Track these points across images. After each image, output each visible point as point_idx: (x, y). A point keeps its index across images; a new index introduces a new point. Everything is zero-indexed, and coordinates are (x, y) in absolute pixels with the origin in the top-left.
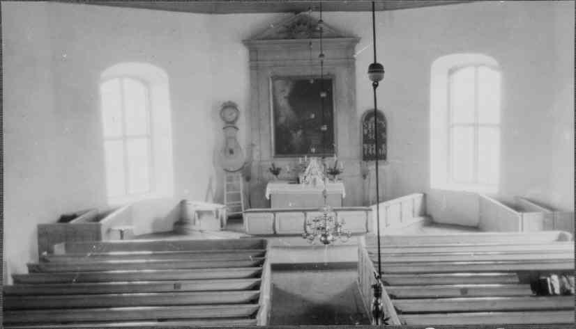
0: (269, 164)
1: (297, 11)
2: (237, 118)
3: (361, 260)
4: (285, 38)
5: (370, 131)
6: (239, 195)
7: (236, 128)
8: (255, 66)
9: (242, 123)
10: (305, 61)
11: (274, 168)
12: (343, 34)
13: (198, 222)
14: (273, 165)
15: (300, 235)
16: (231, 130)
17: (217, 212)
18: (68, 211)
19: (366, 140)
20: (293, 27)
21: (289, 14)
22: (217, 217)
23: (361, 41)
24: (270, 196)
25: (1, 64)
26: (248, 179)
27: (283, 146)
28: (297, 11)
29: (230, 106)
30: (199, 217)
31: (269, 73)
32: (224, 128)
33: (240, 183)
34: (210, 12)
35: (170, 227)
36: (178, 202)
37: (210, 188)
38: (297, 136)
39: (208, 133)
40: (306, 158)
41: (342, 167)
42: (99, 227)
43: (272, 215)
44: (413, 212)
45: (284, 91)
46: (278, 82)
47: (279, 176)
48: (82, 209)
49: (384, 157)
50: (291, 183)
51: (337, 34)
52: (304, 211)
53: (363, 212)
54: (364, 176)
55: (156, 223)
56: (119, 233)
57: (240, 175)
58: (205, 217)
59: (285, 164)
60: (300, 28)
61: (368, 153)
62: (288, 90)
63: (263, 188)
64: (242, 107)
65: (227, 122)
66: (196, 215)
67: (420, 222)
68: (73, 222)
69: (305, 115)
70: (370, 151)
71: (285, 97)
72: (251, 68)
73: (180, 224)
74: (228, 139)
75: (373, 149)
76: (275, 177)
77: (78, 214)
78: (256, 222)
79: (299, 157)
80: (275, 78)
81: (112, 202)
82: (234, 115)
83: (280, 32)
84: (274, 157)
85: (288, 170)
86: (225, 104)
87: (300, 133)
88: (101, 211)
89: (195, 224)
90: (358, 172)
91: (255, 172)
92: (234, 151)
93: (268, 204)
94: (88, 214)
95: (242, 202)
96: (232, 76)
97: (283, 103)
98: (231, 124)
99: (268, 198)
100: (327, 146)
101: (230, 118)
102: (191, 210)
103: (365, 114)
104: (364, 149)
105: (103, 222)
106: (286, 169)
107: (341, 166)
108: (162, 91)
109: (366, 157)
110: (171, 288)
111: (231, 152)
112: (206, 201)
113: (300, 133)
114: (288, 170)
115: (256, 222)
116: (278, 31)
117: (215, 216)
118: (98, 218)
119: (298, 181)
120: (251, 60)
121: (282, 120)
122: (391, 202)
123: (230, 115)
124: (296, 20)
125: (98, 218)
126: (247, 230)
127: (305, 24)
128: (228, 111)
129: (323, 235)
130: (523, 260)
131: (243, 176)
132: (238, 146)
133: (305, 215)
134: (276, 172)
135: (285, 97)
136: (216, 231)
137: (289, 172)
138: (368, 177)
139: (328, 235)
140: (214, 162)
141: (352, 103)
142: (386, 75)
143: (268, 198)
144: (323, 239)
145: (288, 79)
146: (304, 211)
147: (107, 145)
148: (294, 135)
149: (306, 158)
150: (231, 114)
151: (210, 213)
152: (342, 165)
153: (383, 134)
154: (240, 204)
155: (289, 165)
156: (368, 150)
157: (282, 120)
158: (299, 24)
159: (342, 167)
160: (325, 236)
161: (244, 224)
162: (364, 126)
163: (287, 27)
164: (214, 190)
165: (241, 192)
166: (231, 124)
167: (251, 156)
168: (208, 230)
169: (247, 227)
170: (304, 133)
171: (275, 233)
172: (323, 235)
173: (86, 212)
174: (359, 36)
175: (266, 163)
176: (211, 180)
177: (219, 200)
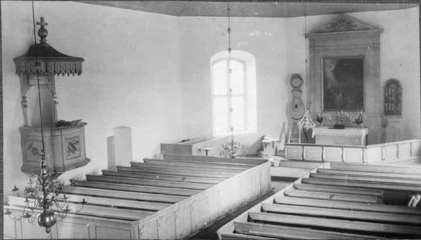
5: (390, 94)
6: (298, 134)
7: (301, 92)
8: (313, 48)
9: (304, 88)
10: (346, 47)
15: (319, 162)
19: (387, 100)
21: (337, 15)
22: (273, 147)
23: (384, 31)
24: (315, 137)
25: (1, 45)
27: (330, 103)
29: (296, 76)
32: (292, 91)
35: (254, 152)
37: (283, 129)
49: (398, 113)
51: (366, 27)
59: (329, 116)
60: (342, 25)
62: (333, 67)
64: (304, 78)
65: (294, 87)
67: (418, 159)
69: (341, 85)
71: (331, 71)
75: (391, 107)
77: (208, 139)
80: (325, 58)
82: (298, 84)
85: (330, 119)
92: (298, 106)
96: (299, 57)
97: (330, 75)
99: (313, 137)
100: (359, 103)
101: (296, 85)
103: (385, 83)
107: (365, 117)
109: (387, 113)
110: (181, 179)
111: (296, 106)
113: (340, 95)
117: (272, 146)
121: (329, 86)
123: (297, 82)
124: (339, 19)
126: (286, 156)
127: (344, 22)
128: (295, 81)
130: (392, 183)
133: (323, 149)
141: (377, 75)
143: (313, 137)
145: (333, 58)
148: (337, 97)
150: (296, 82)
156: (388, 108)
158: (340, 22)
161: (412, 165)
163: (333, 24)
165: (300, 132)
166: (297, 89)
169: (286, 154)
170: (343, 95)
171: (303, 159)
176: (284, 124)
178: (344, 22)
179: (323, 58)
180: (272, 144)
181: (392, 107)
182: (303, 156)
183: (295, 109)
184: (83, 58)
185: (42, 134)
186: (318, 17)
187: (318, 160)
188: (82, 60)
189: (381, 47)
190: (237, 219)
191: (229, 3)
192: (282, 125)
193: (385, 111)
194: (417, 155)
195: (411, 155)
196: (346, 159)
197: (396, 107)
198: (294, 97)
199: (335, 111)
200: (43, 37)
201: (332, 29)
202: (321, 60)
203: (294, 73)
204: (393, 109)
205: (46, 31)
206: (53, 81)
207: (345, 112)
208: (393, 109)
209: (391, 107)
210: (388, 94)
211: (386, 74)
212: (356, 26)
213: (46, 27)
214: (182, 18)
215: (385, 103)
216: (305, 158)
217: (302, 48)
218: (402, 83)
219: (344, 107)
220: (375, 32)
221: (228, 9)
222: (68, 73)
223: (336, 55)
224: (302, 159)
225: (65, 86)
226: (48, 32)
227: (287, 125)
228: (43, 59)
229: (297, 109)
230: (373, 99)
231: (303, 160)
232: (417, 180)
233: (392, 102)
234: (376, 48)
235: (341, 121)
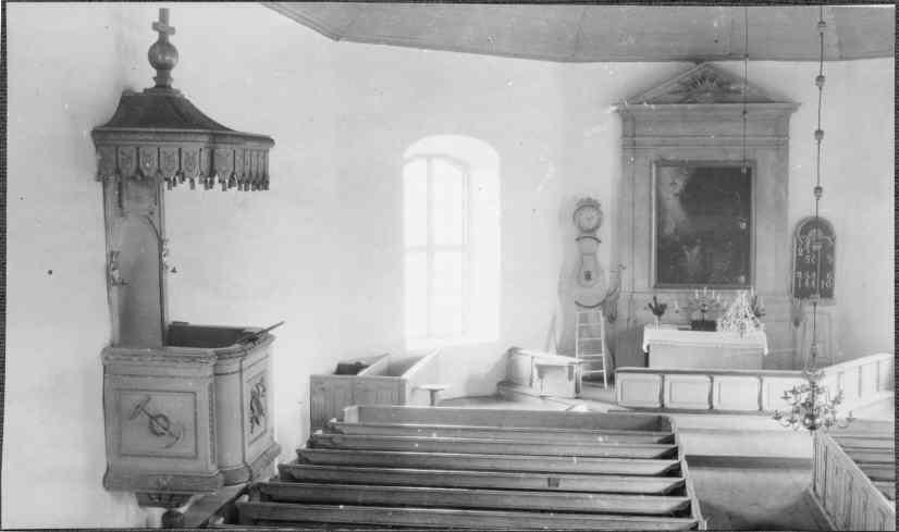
0: (649, 298)
1: (698, 60)
2: (597, 227)
3: (820, 457)
4: (680, 102)
6: (599, 342)
8: (631, 142)
9: (606, 232)
10: (714, 138)
11: (656, 303)
12: (773, 98)
13: (537, 383)
14: (655, 298)
16: (588, 244)
17: (571, 368)
18: (350, 359)
19: (801, 265)
20: (694, 84)
22: (570, 378)
24: (648, 348)
26: (612, 319)
27: (671, 266)
28: (698, 60)
29: (590, 204)
30: (541, 376)
31: (653, 155)
32: (578, 239)
33: (599, 321)
34: (565, 60)
35: (491, 389)
36: (505, 350)
38: (692, 255)
39: (551, 251)
40: (705, 291)
41: (763, 306)
42: (402, 384)
43: (658, 377)
44: (878, 381)
45: (674, 184)
46: (666, 171)
47: (664, 317)
48: (378, 352)
49: (827, 294)
50: (680, 329)
52: (711, 374)
53: (754, 380)
54: (797, 324)
55: (471, 381)
56: (429, 393)
57: (601, 312)
58: (548, 378)
59: (672, 298)
60: (705, 83)
61: (803, 287)
62: (680, 184)
63: (637, 334)
66: (535, 372)
68: (361, 374)
69: (706, 220)
70: (807, 283)
72: (624, 147)
73: (507, 385)
74: (584, 256)
75: (810, 281)
76: (656, 317)
77: (363, 362)
78: (635, 390)
79: (695, 288)
80: (662, 163)
81: (412, 347)
83: (674, 92)
84: (655, 287)
85: (677, 307)
86: (582, 201)
87: (696, 250)
88: (396, 356)
89: (531, 384)
90: (787, 315)
91: (623, 312)
92: (593, 275)
93: (646, 360)
94: (379, 362)
95: (603, 354)
96: (599, 165)
97: (672, 203)
98: (588, 234)
102: (526, 365)
103: (800, 223)
104: (797, 279)
105: (407, 376)
106: (674, 307)
108: (488, 181)
109: (801, 292)
111: (588, 276)
112: (547, 349)
113: (696, 250)
114: (677, 307)
115: (635, 390)
116: (669, 89)
117: (567, 375)
118: (395, 370)
119: (710, 326)
120: (624, 135)
122: (846, 365)
124: (699, 74)
125: (395, 370)
127: (712, 80)
129: (807, 416)
131: (604, 314)
132: (599, 271)
134: (659, 310)
135: (676, 195)
136: (569, 398)
137: (677, 312)
138: (801, 323)
139: (818, 416)
140: (560, 292)
141: (781, 206)
142: (825, 137)
144: (807, 421)
146: (711, 374)
147: (413, 263)
149: (705, 291)
151: (560, 368)
152: (762, 303)
153: (829, 257)
154: (600, 358)
155: (679, 300)
156: (803, 281)
157: (669, 230)
158: (703, 79)
159: (763, 306)
160: (812, 417)
162: (798, 242)
163: (684, 84)
164: (558, 339)
165: (602, 338)
166: (588, 234)
167: (618, 284)
168: (552, 395)
170: (702, 250)
172: (807, 416)
173: (379, 358)
174: (799, 101)
175: (641, 297)
176: (554, 319)
177: (565, 350)
178: (712, 80)
179: (656, 162)
180: (567, 369)
181: (811, 280)
182: (710, 402)
183: (584, 282)
184: (273, 137)
185: (233, 373)
186: (653, 65)
187: (887, 436)
188: (268, 141)
189: (791, 143)
190: (234, 490)
191: (824, 7)
192: (550, 318)
193: (796, 288)
194: (888, 389)
195: (878, 389)
196: (769, 404)
197: (821, 279)
198: (583, 255)
199: (690, 288)
200: (163, 69)
201: (679, 97)
202: (651, 168)
203: (585, 197)
204: (813, 283)
205: (171, 50)
206: (157, 199)
207: (713, 291)
208: (813, 283)
209: (810, 281)
210: (805, 252)
211: (801, 206)
212: (737, 92)
213: (172, 39)
214: (345, 46)
215: (797, 270)
216: (668, 404)
217: (605, 132)
218: (837, 229)
219: (703, 279)
220: (775, 111)
221: (822, 22)
222: (192, 181)
223: (688, 156)
224: (707, 407)
225: (191, 209)
226: (180, 52)
227: (560, 320)
228: (152, 135)
229: (591, 283)
230: (772, 260)
231: (712, 410)
232: (884, 451)
233: (812, 268)
234: (780, 144)
235: (703, 311)
